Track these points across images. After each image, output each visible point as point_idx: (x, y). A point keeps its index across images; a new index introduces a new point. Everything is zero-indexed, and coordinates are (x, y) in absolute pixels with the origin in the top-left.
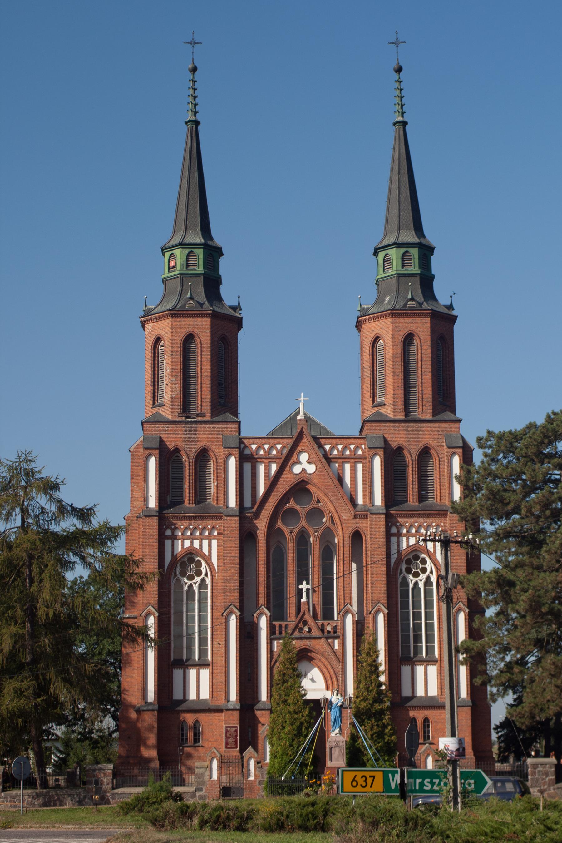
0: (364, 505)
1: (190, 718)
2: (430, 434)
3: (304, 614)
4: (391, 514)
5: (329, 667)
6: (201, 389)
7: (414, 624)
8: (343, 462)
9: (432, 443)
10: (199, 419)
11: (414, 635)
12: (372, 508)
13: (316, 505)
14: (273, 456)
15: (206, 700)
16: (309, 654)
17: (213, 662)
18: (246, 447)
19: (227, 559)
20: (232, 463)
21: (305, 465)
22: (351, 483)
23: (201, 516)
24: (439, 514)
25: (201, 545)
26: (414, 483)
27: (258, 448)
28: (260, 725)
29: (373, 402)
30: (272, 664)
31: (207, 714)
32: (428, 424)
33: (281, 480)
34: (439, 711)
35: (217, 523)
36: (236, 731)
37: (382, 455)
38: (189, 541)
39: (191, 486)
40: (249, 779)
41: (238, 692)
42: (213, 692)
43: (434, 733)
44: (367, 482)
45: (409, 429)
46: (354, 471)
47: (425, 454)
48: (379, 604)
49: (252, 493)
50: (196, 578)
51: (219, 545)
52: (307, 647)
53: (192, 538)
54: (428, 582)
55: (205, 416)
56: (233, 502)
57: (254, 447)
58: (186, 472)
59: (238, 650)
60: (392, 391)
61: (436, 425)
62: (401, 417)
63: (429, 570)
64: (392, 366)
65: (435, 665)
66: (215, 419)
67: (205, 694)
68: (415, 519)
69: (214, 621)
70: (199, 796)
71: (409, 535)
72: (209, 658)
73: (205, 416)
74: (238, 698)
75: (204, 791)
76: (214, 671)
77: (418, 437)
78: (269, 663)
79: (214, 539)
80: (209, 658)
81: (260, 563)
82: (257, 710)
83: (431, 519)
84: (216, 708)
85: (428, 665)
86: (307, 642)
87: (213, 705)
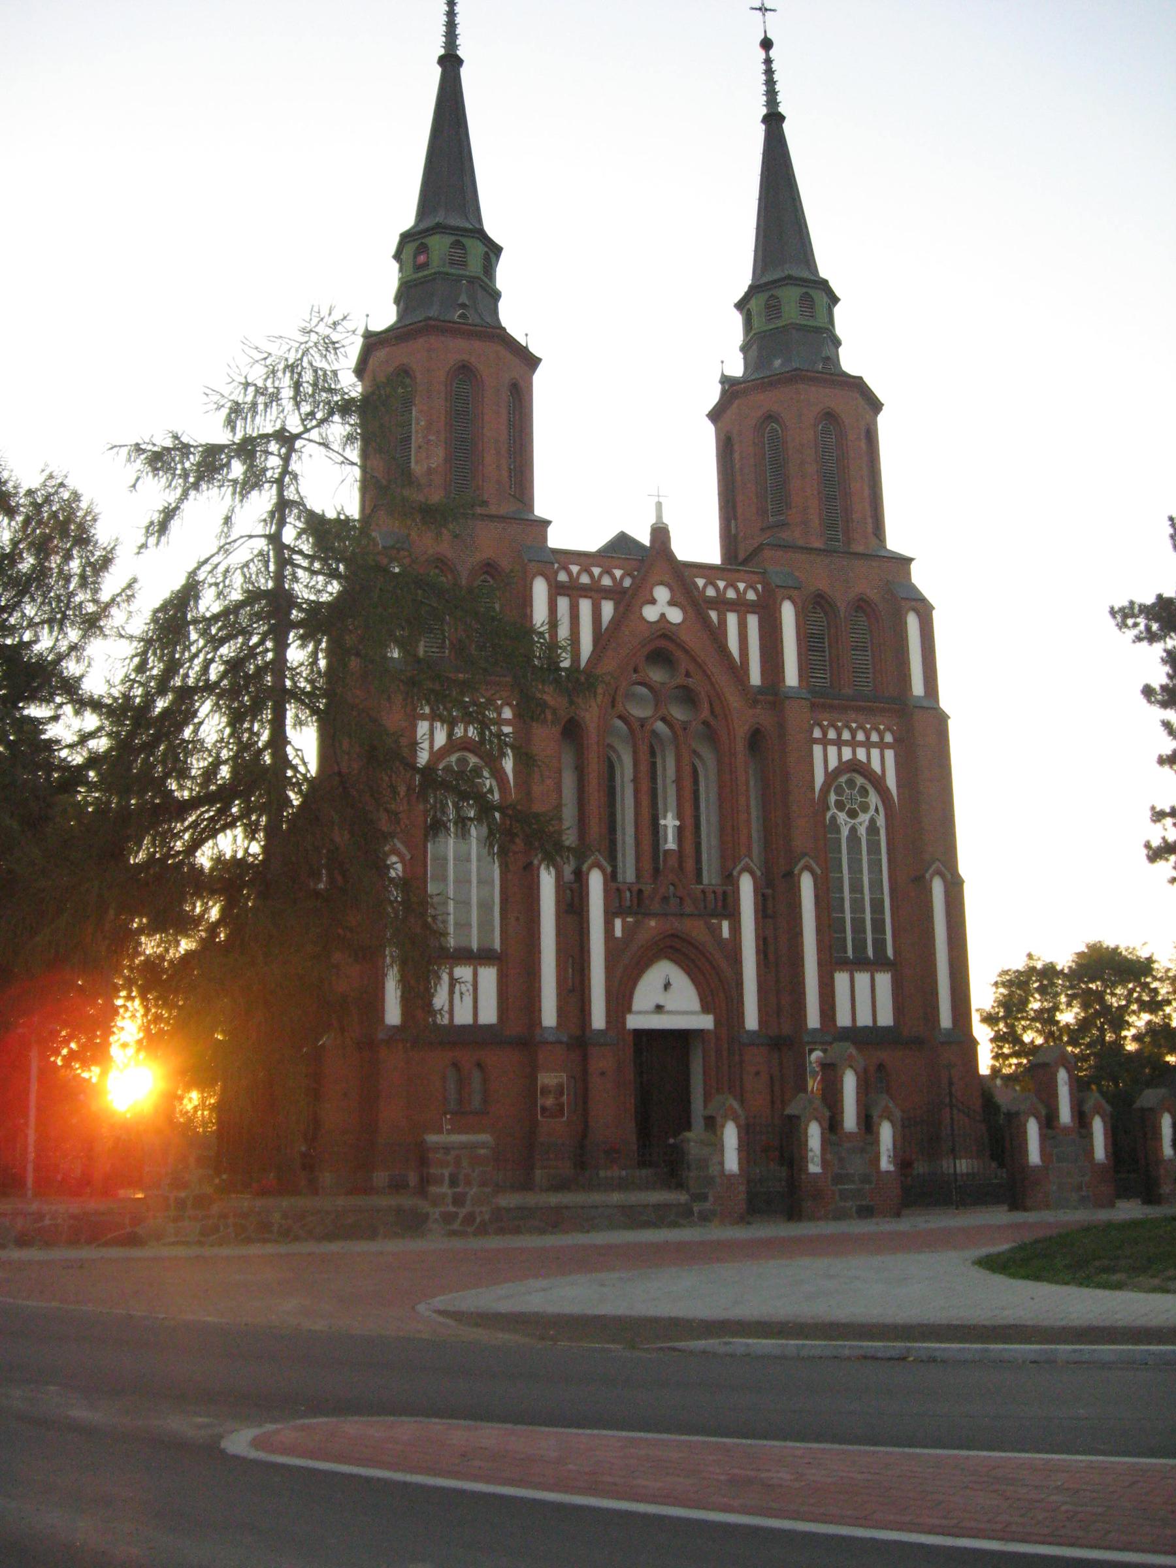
54: (873, 829)
63: (872, 808)
75: (711, 1199)
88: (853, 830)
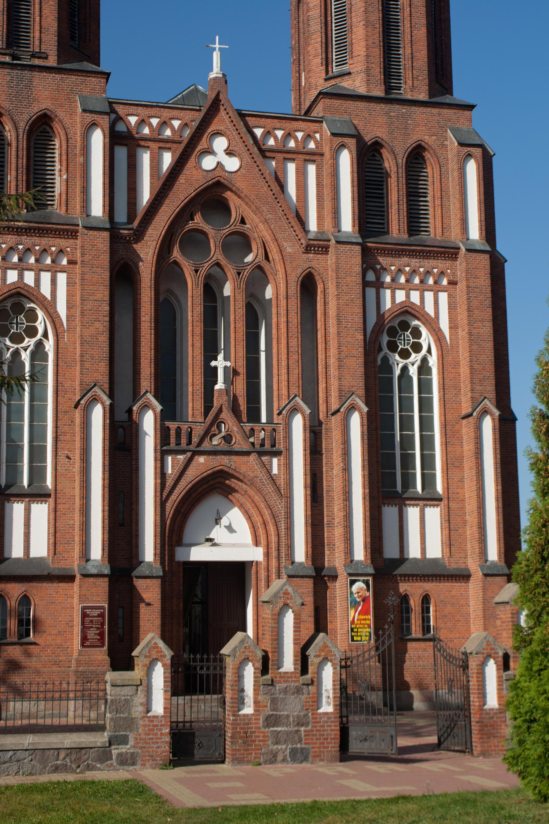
0: (321, 231)
1: (14, 591)
2: (426, 125)
3: (220, 410)
4: (368, 247)
5: (262, 505)
6: (41, 11)
7: (401, 435)
8: (285, 159)
9: (429, 140)
10: (37, 62)
11: (402, 454)
12: (339, 234)
13: (239, 227)
14: (166, 137)
15: (41, 559)
16: (227, 482)
17: (56, 490)
18: (119, 118)
19: (88, 305)
20: (98, 139)
21: (220, 157)
22: (297, 196)
23: (39, 229)
24: (444, 253)
25: (37, 280)
26: (401, 202)
27: (142, 122)
28: (142, 605)
29: (327, 72)
30: (164, 496)
31: (44, 584)
32: (422, 109)
33: (182, 179)
34: (447, 584)
35: (67, 244)
36: (102, 615)
37: (354, 148)
38: (16, 272)
39: (20, 177)
40: (241, 712)
41: (107, 544)
42: (55, 544)
43: (440, 622)
44: (325, 193)
45: (392, 114)
46: (302, 176)
47: (416, 157)
48: (353, 396)
49: (129, 198)
50: (27, 340)
51: (70, 283)
52: (226, 469)
53: (21, 268)
54: (424, 368)
55: (46, 58)
56: (97, 209)
57: (133, 120)
58: (12, 154)
59: (107, 468)
60: (364, 49)
61: (435, 111)
62: (379, 92)
64: (363, 9)
65: (437, 506)
66: (64, 66)
67: (40, 549)
68: (405, 260)
69: (60, 416)
70: (120, 755)
71: (394, 286)
72: (49, 482)
73: (46, 58)
74: (106, 554)
75: (131, 742)
76: (59, 507)
77: (406, 128)
78: (158, 494)
79: (61, 271)
80: (49, 482)
81: (143, 319)
82: (137, 577)
83: (432, 262)
84: (62, 573)
85: (426, 505)
86: (224, 460)
87: (55, 567)
88: (405, 369)
